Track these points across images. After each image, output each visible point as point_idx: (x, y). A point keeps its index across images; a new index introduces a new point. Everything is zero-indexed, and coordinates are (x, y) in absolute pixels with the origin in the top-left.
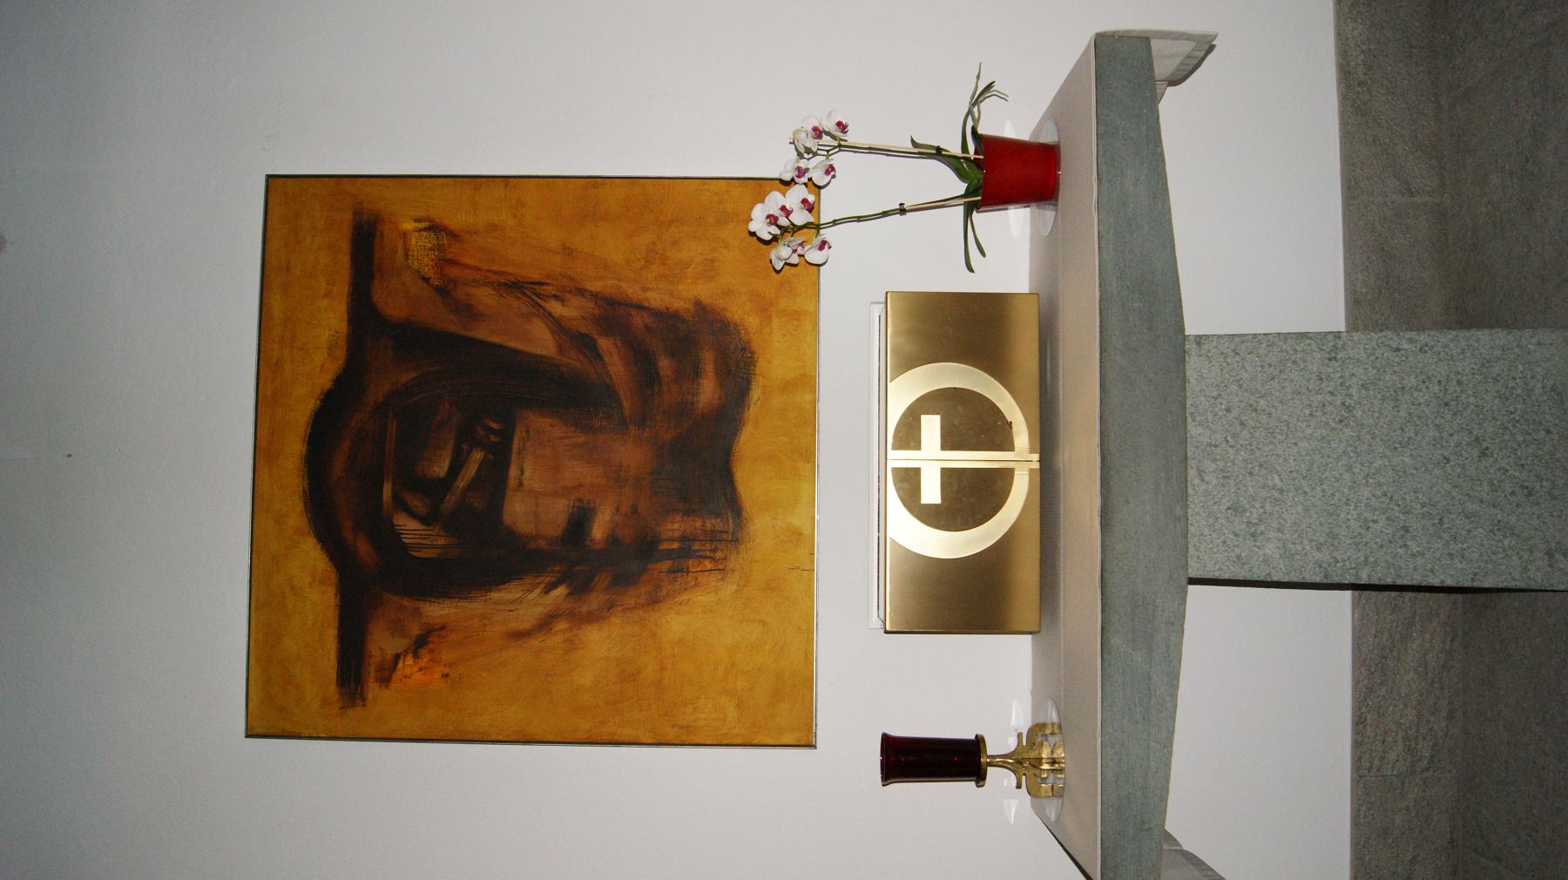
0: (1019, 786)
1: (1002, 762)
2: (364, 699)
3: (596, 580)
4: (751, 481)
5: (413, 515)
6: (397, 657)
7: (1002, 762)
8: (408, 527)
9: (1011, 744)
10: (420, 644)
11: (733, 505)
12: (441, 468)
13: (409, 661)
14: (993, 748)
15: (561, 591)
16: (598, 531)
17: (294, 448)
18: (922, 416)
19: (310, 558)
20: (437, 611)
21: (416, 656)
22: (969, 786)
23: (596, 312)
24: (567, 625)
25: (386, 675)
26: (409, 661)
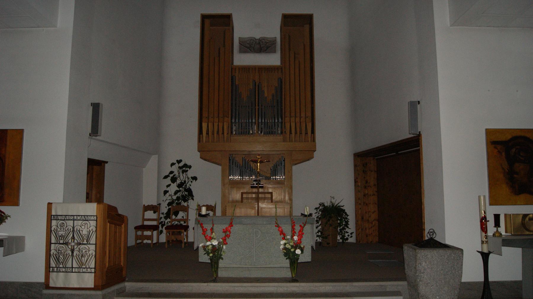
0: (494, 232)
1: (497, 230)
2: (492, 144)
3: (177, 223)
4: (523, 196)
5: (515, 150)
6: (497, 149)
7: (497, 230)
8: (514, 150)
9: (499, 231)
10: (499, 152)
11: (520, 194)
12: (522, 154)
13: (497, 151)
14: (499, 228)
15: (507, 171)
16: (515, 176)
17: (522, 134)
18: (310, 260)
19: (509, 137)
20: (503, 154)
21: (498, 151)
22: (494, 225)
23: (328, 206)
24: (367, 191)
25: (495, 148)
26: (497, 151)
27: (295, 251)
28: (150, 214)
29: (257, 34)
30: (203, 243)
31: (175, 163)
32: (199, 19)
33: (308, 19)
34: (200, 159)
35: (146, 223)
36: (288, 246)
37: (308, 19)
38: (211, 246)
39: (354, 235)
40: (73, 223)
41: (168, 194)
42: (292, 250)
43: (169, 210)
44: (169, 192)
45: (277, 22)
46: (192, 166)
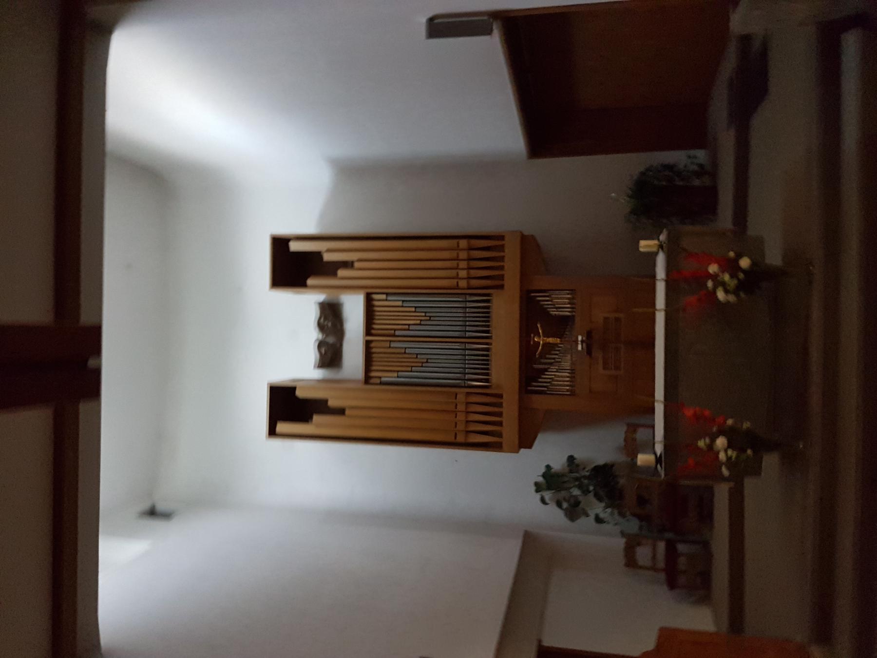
27: (744, 271)
28: (643, 554)
29: (311, 335)
30: (721, 469)
31: (541, 495)
32: (277, 443)
33: (280, 244)
34: (534, 447)
35: (661, 564)
36: (732, 283)
37: (280, 244)
38: (730, 452)
39: (692, 152)
40: (537, 396)
41: (602, 515)
42: (741, 276)
43: (634, 515)
44: (598, 512)
45: (287, 297)
46: (546, 464)
